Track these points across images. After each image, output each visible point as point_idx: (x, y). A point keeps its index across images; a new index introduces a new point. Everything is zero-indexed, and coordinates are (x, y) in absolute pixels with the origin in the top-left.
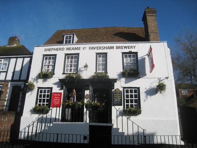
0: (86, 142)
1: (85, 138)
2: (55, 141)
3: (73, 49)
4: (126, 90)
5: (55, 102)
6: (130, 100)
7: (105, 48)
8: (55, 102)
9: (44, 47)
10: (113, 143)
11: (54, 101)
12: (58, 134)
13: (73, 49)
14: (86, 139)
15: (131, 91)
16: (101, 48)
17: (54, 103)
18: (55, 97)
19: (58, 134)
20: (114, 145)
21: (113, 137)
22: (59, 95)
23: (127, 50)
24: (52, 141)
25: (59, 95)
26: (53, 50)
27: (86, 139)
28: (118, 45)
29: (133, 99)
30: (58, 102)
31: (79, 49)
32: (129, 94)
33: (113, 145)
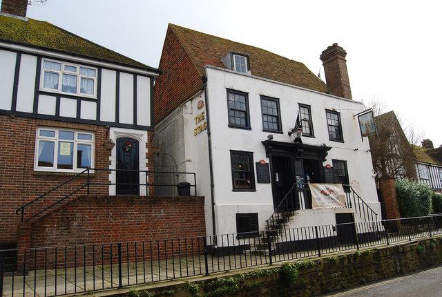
12: (316, 227)
19: (316, 227)
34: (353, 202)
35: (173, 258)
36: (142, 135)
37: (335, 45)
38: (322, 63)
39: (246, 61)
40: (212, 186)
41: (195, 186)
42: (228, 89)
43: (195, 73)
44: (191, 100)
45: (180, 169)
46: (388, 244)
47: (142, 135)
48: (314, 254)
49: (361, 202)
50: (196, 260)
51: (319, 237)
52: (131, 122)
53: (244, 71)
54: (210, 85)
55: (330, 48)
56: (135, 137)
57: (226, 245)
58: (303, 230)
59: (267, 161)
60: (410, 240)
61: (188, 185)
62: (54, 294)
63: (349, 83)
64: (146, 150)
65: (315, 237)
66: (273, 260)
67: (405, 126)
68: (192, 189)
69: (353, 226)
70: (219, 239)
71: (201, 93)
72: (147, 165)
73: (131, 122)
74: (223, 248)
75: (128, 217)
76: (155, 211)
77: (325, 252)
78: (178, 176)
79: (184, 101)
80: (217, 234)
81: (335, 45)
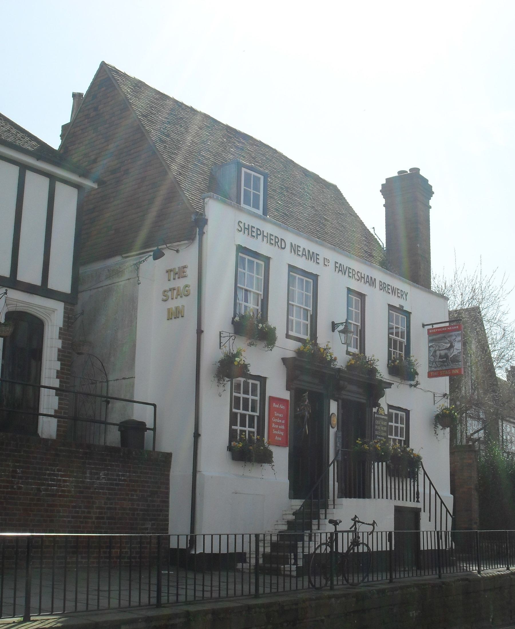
18: (276, 414)
22: (282, 407)
23: (396, 302)
34: (421, 490)
36: (54, 311)
39: (406, 319)
40: (197, 435)
41: (154, 429)
42: (389, 305)
45: (114, 389)
47: (54, 311)
49: (433, 492)
52: (38, 282)
53: (239, 202)
54: (210, 229)
56: (40, 314)
57: (208, 551)
60: (391, 581)
61: (140, 427)
64: (59, 344)
65: (388, 549)
67: (433, 188)
68: (148, 434)
70: (199, 540)
72: (60, 375)
73: (38, 282)
74: (203, 554)
75: (47, 480)
76: (91, 473)
78: (108, 402)
80: (197, 532)
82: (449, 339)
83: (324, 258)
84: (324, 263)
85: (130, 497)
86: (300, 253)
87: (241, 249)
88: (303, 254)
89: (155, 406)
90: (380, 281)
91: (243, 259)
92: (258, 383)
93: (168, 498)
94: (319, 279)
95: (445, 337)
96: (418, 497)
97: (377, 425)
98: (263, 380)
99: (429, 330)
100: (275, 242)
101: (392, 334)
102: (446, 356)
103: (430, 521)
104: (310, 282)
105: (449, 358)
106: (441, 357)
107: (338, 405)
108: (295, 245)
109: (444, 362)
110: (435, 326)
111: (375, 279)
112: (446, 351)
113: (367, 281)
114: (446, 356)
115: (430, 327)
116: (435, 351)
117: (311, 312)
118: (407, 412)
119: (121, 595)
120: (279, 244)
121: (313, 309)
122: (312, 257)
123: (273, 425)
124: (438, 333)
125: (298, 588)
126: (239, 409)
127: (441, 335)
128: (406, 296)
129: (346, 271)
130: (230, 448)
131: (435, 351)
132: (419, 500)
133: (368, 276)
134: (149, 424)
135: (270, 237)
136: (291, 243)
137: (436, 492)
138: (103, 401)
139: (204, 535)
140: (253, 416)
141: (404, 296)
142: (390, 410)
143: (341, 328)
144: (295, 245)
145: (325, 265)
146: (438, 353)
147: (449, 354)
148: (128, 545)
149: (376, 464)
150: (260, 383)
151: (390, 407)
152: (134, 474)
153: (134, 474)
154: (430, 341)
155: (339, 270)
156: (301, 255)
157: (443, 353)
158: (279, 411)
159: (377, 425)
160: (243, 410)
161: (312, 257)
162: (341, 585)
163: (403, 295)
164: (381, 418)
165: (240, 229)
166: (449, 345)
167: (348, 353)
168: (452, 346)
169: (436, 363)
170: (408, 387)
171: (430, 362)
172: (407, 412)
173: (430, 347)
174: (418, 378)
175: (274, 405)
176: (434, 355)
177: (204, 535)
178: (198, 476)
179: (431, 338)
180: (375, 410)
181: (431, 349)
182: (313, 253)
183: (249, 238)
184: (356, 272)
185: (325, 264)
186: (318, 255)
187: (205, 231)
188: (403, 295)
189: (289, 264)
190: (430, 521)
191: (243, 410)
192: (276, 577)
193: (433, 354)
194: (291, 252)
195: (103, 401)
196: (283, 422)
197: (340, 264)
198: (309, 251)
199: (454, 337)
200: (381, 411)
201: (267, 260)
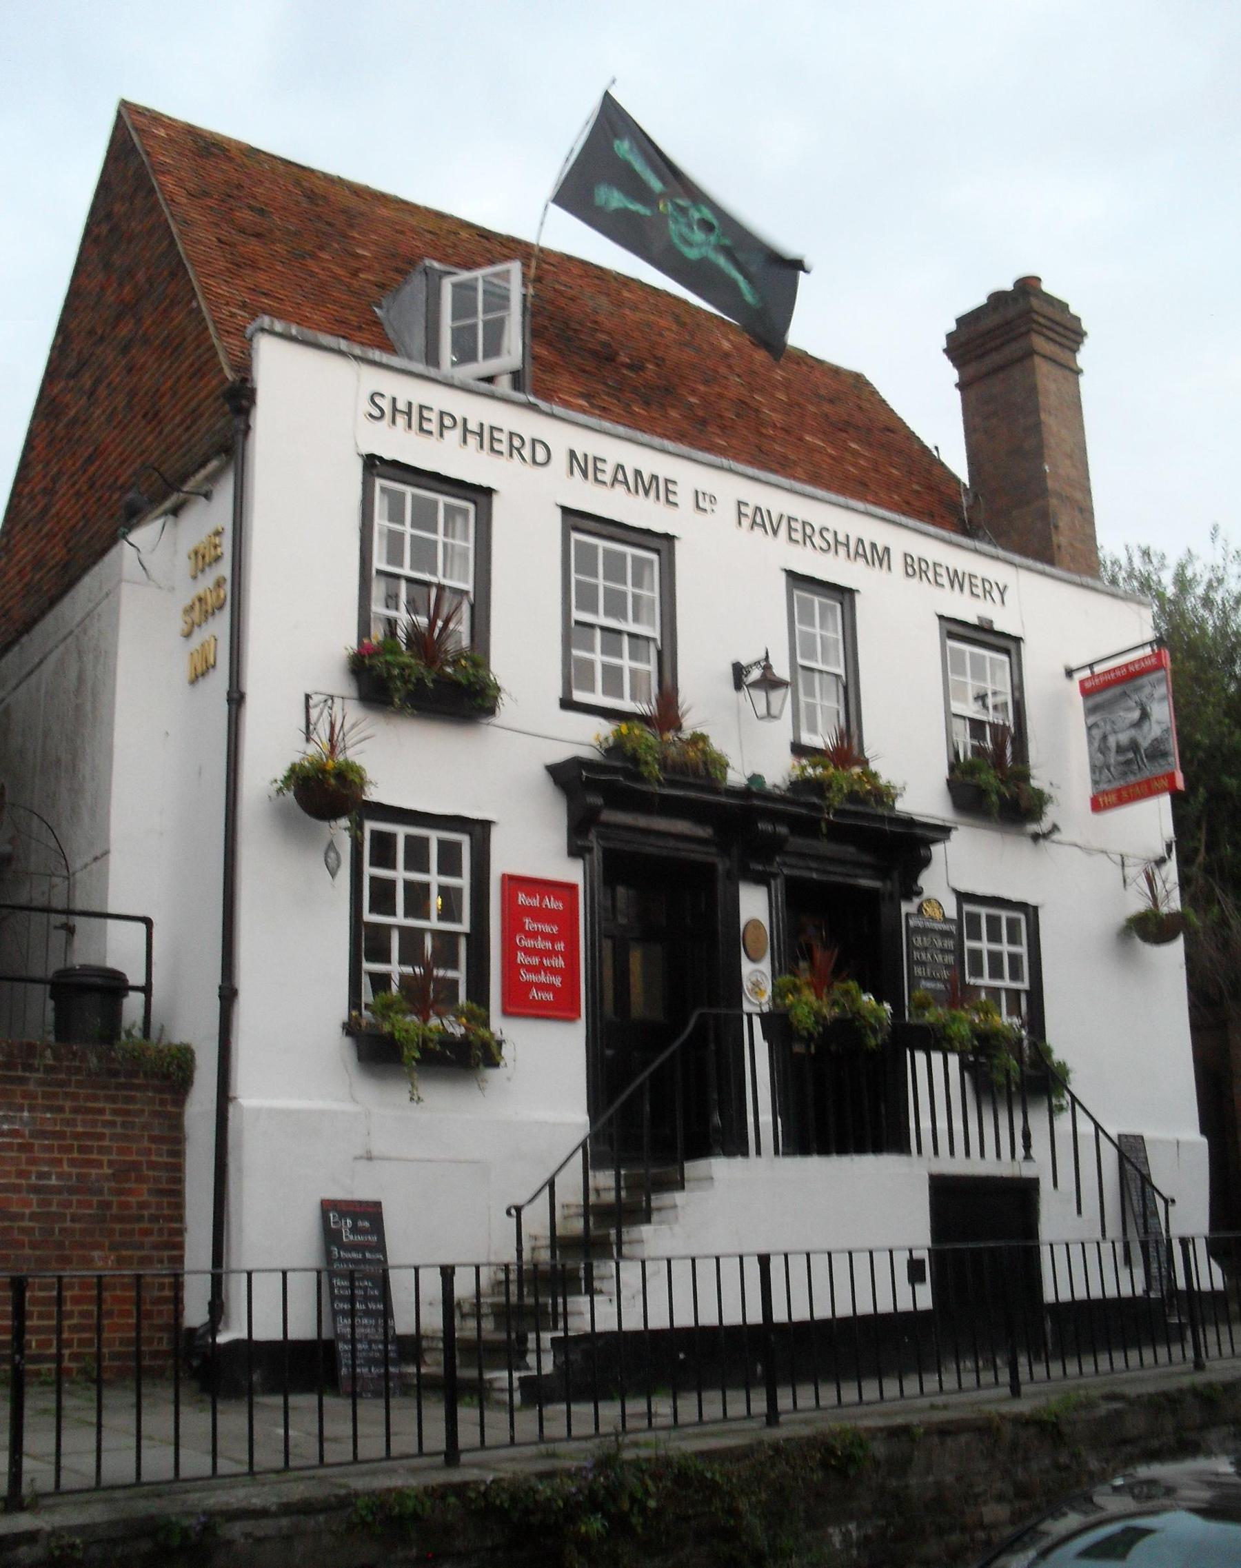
0: (925, 1298)
1: (915, 1271)
2: (755, 1316)
3: (619, 476)
4: (373, 832)
5: (530, 969)
6: (403, 930)
7: (395, 410)
8: (530, 969)
9: (367, 372)
10: (1049, 1296)
11: (521, 957)
12: (764, 1260)
13: (619, 476)
14: (923, 1280)
15: (417, 858)
16: (817, 540)
17: (526, 977)
18: (529, 924)
19: (764, 1260)
20: (1057, 1306)
21: (1045, 1251)
22: (552, 904)
23: (968, 610)
24: (732, 1318)
25: (552, 904)
26: (454, 436)
27: (923, 1280)
28: (590, 443)
29: (389, 927)
30: (553, 971)
31: (879, 556)
32: (400, 875)
33: (782, 1325)
35: (58, 1383)
37: (1028, 286)
38: (953, 375)
40: (228, 995)
41: (147, 989)
42: (566, 511)
43: (209, 361)
44: (175, 511)
46: (452, 1455)
48: (737, 1407)
50: (119, 1403)
51: (779, 1315)
53: (432, 357)
55: (997, 299)
58: (841, 1263)
59: (573, 873)
62: (170, 1475)
63: (1088, 492)
66: (784, 1401)
68: (133, 1004)
69: (1031, 1257)
71: (214, 478)
77: (806, 1396)
78: (70, 930)
79: (133, 516)
81: (1028, 286)
82: (1136, 697)
83: (697, 492)
84: (697, 502)
85: (33, 1180)
86: (607, 478)
87: (373, 465)
88: (615, 479)
89: (148, 922)
90: (906, 555)
91: (587, 553)
92: (465, 840)
93: (180, 1181)
94: (679, 547)
95: (1125, 694)
96: (1027, 1146)
97: (917, 949)
98: (480, 830)
99: (1082, 682)
100: (511, 445)
101: (588, 600)
102: (1134, 746)
103: (1079, 1211)
104: (651, 562)
105: (1142, 751)
106: (1120, 750)
107: (585, 865)
108: (586, 456)
109: (1128, 763)
110: (1098, 669)
111: (887, 550)
112: (1133, 732)
113: (857, 553)
114: (1134, 746)
115: (1086, 673)
116: (1105, 738)
117: (659, 643)
118: (1031, 912)
119: (291, 1457)
120: (526, 452)
121: (475, 588)
122: (647, 485)
123: (521, 957)
124: (1108, 685)
125: (681, 1419)
126: (393, 913)
127: (1116, 690)
128: (1002, 594)
129: (636, 480)
130: (351, 1028)
131: (1105, 738)
132: (1033, 1152)
133: (860, 541)
134: (136, 977)
135: (595, 464)
136: (572, 454)
137: (1098, 1127)
138: (56, 928)
139: (249, 1274)
140: (454, 935)
141: (996, 594)
142: (967, 908)
143: (756, 674)
144: (586, 456)
145: (698, 506)
146: (1112, 741)
147: (1140, 740)
148: (130, 1321)
149: (920, 1057)
150: (471, 839)
151: (963, 897)
152: (48, 1115)
153: (48, 1115)
154: (1090, 711)
155: (754, 522)
156: (801, 540)
157: (1124, 738)
158: (540, 914)
159: (917, 949)
160: (407, 914)
161: (647, 485)
162: (809, 1410)
163: (988, 589)
164: (933, 930)
165: (377, 413)
166: (1136, 715)
167: (798, 749)
168: (1145, 715)
169: (1109, 770)
170: (1028, 842)
171: (1094, 769)
172: (1031, 912)
173: (1089, 728)
174: (1051, 815)
175: (522, 899)
176: (1103, 749)
177: (249, 1274)
178: (232, 1110)
179: (1091, 702)
180: (906, 908)
181: (1095, 732)
182: (654, 478)
183: (414, 437)
184: (931, 565)
185: (701, 504)
186: (674, 483)
187: (251, 423)
188: (988, 589)
189: (786, 571)
190: (1079, 1211)
191: (407, 914)
192: (742, 1395)
193: (1099, 745)
194: (572, 472)
195: (56, 928)
196: (560, 946)
197: (758, 509)
198: (874, 546)
199: (1147, 690)
200: (929, 910)
201: (481, 495)
